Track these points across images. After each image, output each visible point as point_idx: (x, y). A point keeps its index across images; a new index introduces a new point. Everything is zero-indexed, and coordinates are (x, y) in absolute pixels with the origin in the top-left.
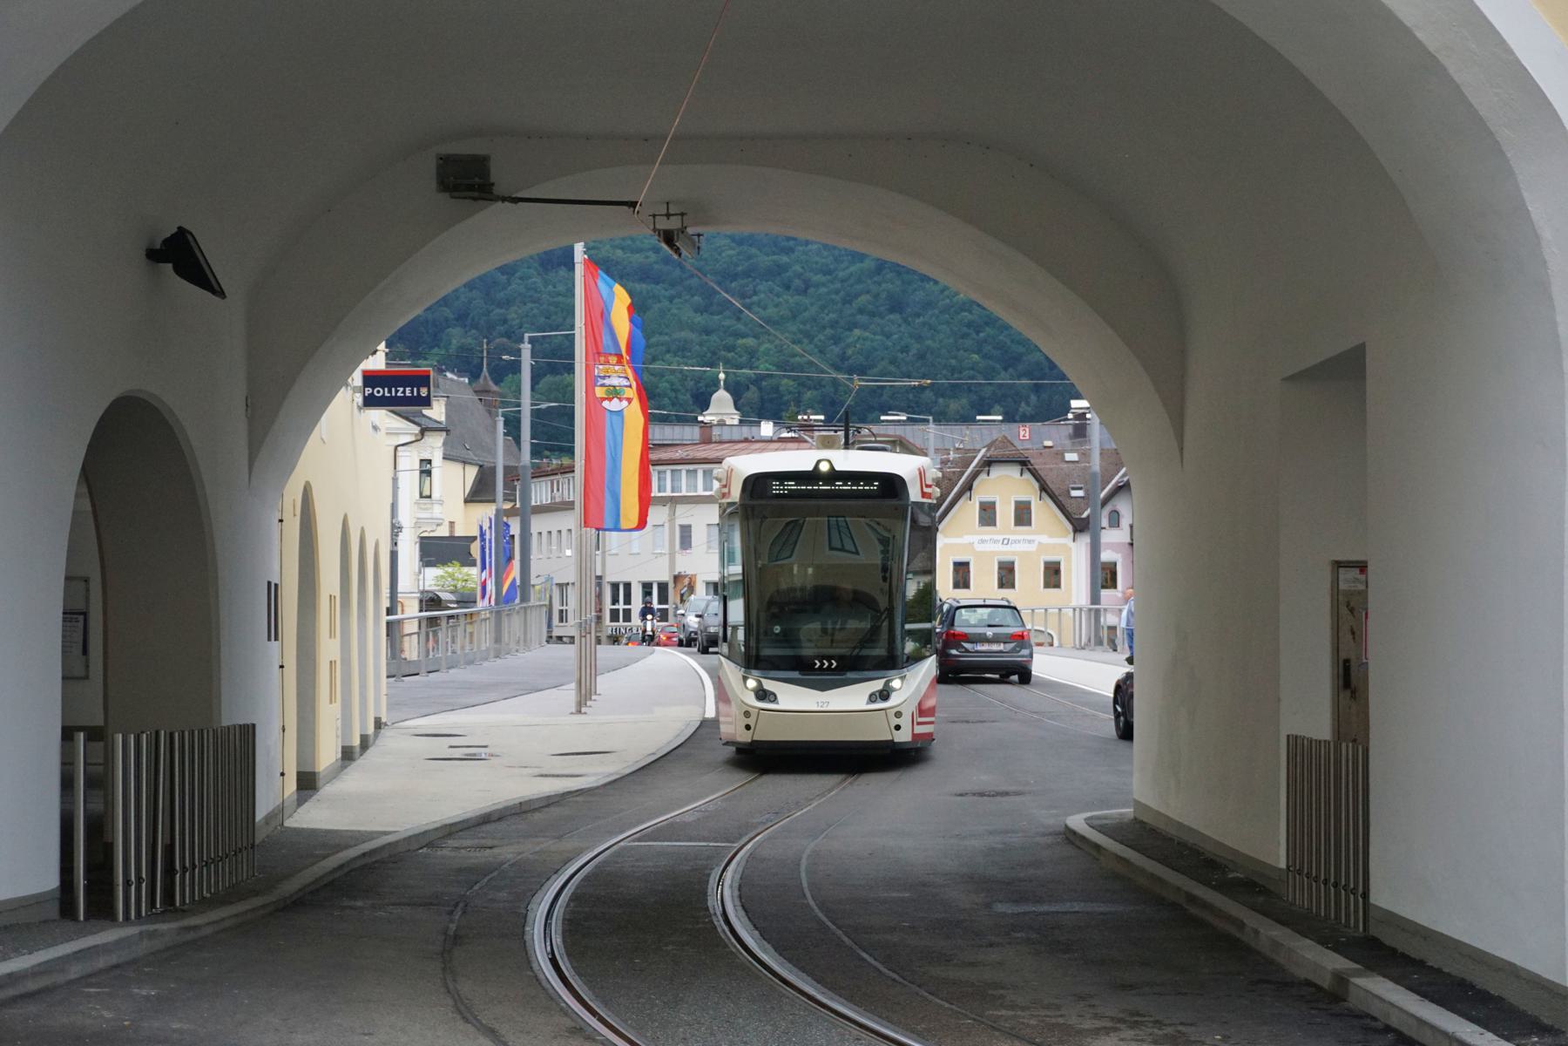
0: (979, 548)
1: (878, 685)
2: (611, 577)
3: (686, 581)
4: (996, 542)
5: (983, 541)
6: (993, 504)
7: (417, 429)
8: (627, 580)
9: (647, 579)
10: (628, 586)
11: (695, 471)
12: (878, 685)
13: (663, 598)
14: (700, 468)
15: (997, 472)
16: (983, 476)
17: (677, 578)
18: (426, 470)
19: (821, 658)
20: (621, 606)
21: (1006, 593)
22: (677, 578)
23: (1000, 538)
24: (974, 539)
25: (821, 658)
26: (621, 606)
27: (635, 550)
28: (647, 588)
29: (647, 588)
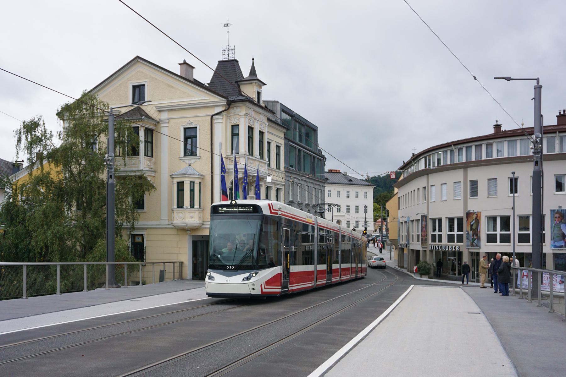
1: (247, 275)
2: (431, 216)
3: (474, 217)
10: (440, 220)
11: (481, 145)
12: (247, 275)
13: (460, 228)
14: (464, 147)
17: (469, 214)
19: (229, 266)
22: (469, 214)
25: (229, 266)
26: (437, 233)
27: (444, 199)
28: (451, 220)
29: (451, 220)
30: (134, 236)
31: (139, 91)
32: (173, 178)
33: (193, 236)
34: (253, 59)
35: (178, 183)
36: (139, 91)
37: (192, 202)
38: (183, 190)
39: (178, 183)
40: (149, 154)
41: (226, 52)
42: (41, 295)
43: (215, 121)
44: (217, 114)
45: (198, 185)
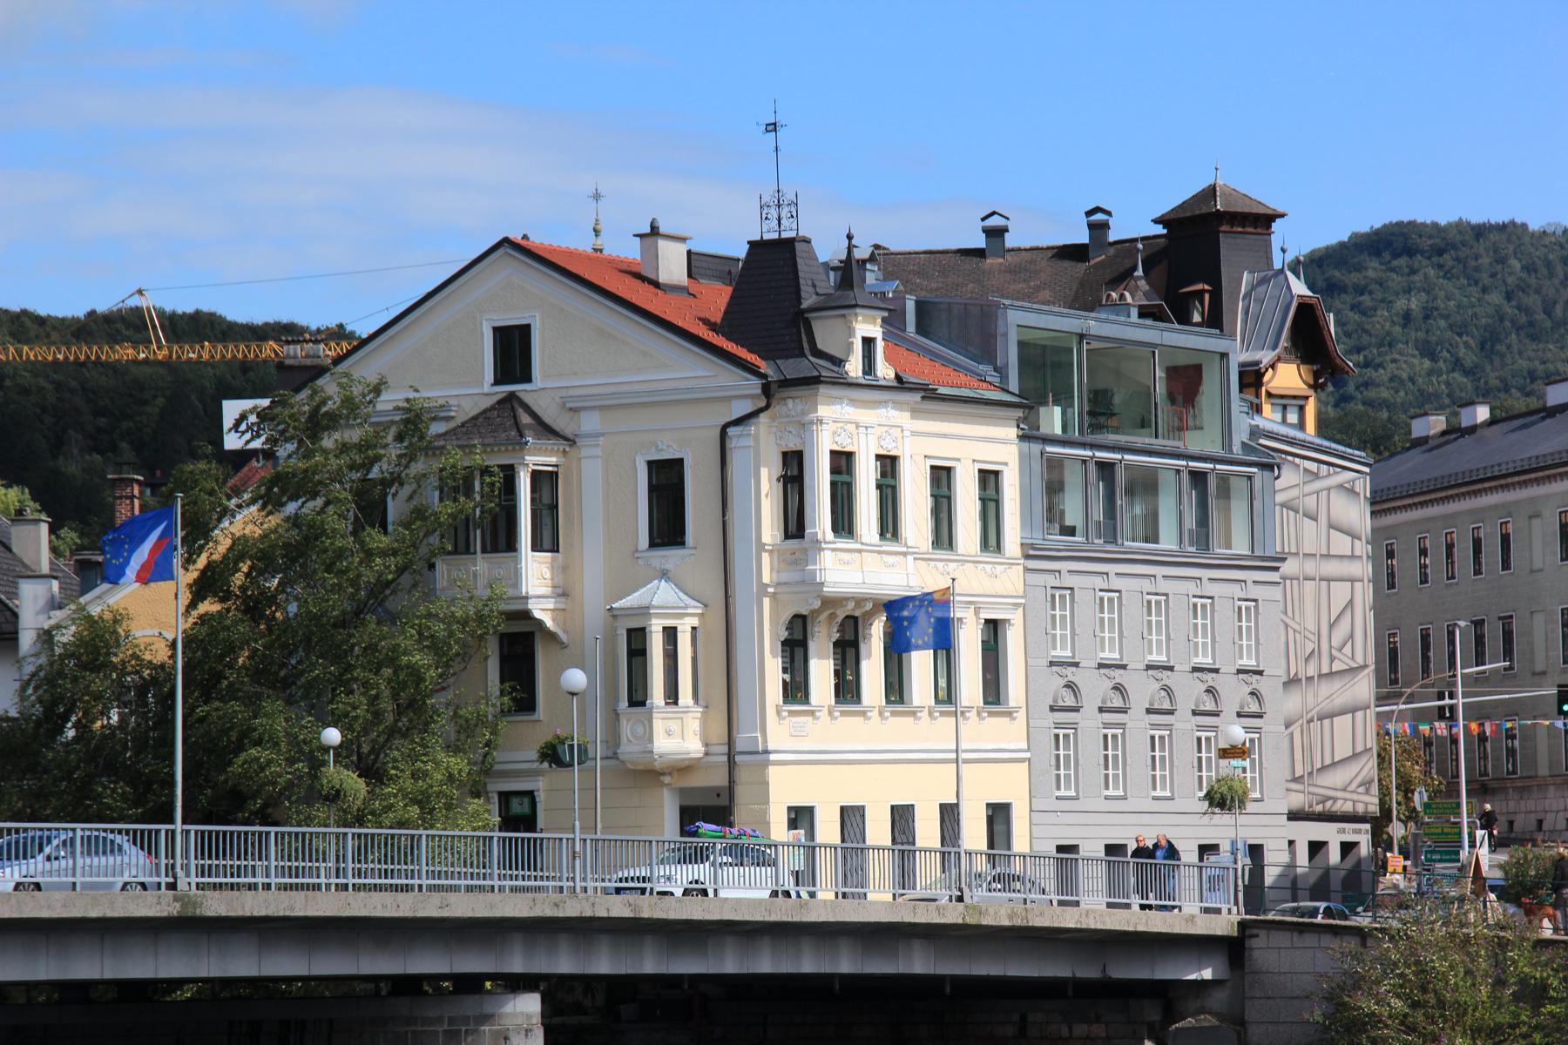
30: (505, 797)
31: (513, 352)
32: (614, 617)
33: (683, 792)
34: (850, 237)
35: (630, 631)
36: (513, 352)
37: (895, 680)
38: (998, 502)
39: (630, 631)
40: (547, 543)
41: (774, 213)
42: (1037, 249)
43: (732, 444)
44: (738, 422)
45: (688, 636)
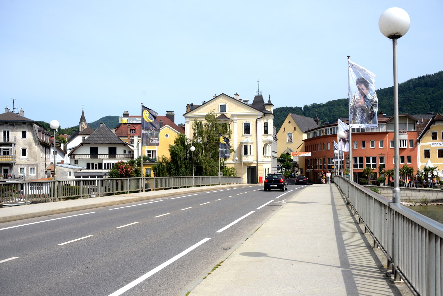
0: (432, 146)
4: (437, 144)
5: (433, 144)
6: (436, 133)
7: (262, 114)
8: (374, 156)
9: (368, 156)
15: (436, 124)
16: (433, 125)
18: (266, 125)
20: (342, 164)
21: (245, 121)
23: (438, 143)
24: (431, 143)
